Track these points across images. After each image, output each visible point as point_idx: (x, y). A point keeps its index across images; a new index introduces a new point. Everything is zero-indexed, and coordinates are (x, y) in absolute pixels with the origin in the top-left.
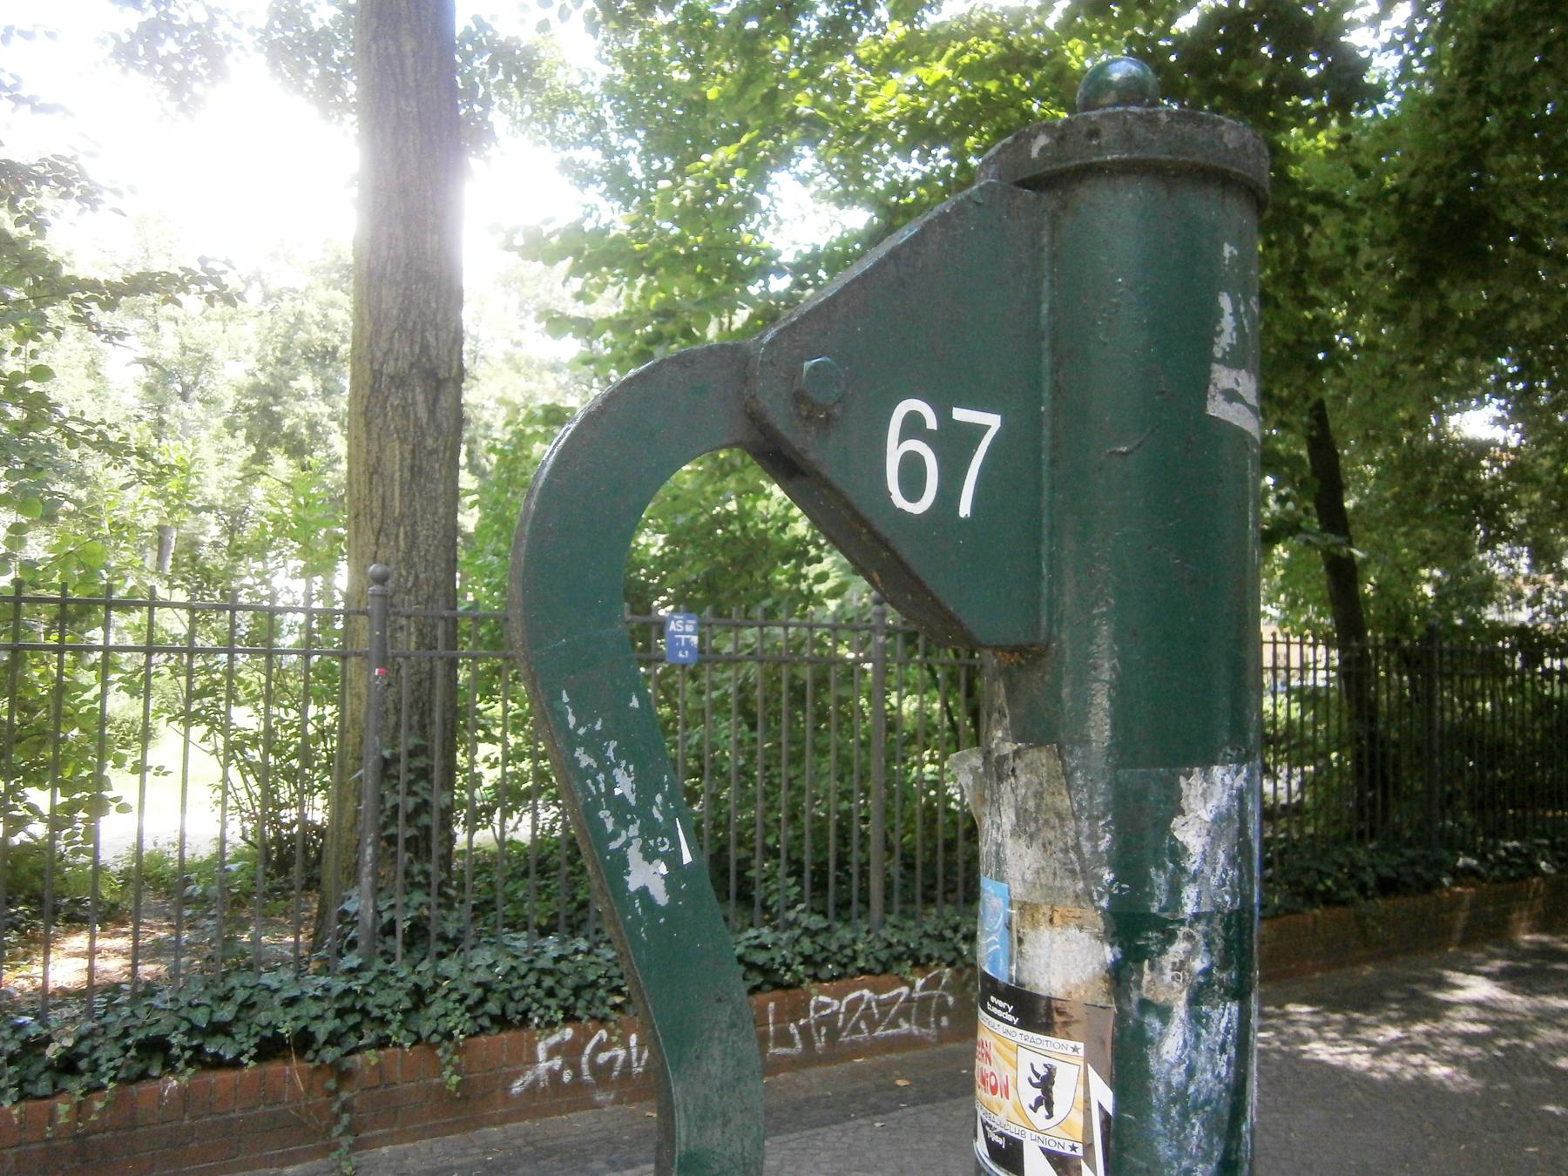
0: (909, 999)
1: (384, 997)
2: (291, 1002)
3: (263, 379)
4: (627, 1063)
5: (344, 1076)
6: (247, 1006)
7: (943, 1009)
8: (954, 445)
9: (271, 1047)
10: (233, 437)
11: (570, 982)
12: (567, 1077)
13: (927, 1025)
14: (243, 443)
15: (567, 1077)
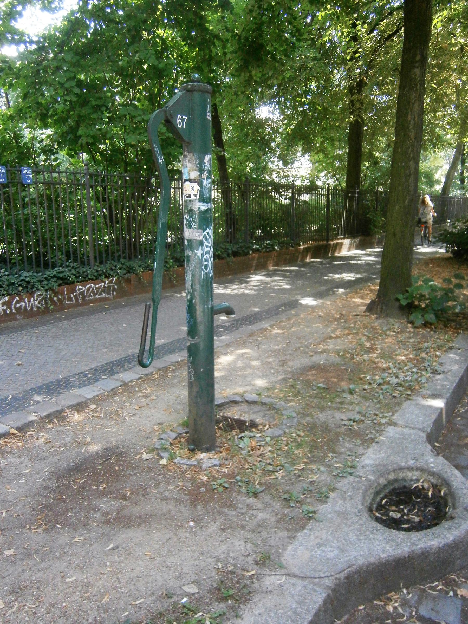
0: (104, 287)
4: (25, 307)
7: (114, 290)
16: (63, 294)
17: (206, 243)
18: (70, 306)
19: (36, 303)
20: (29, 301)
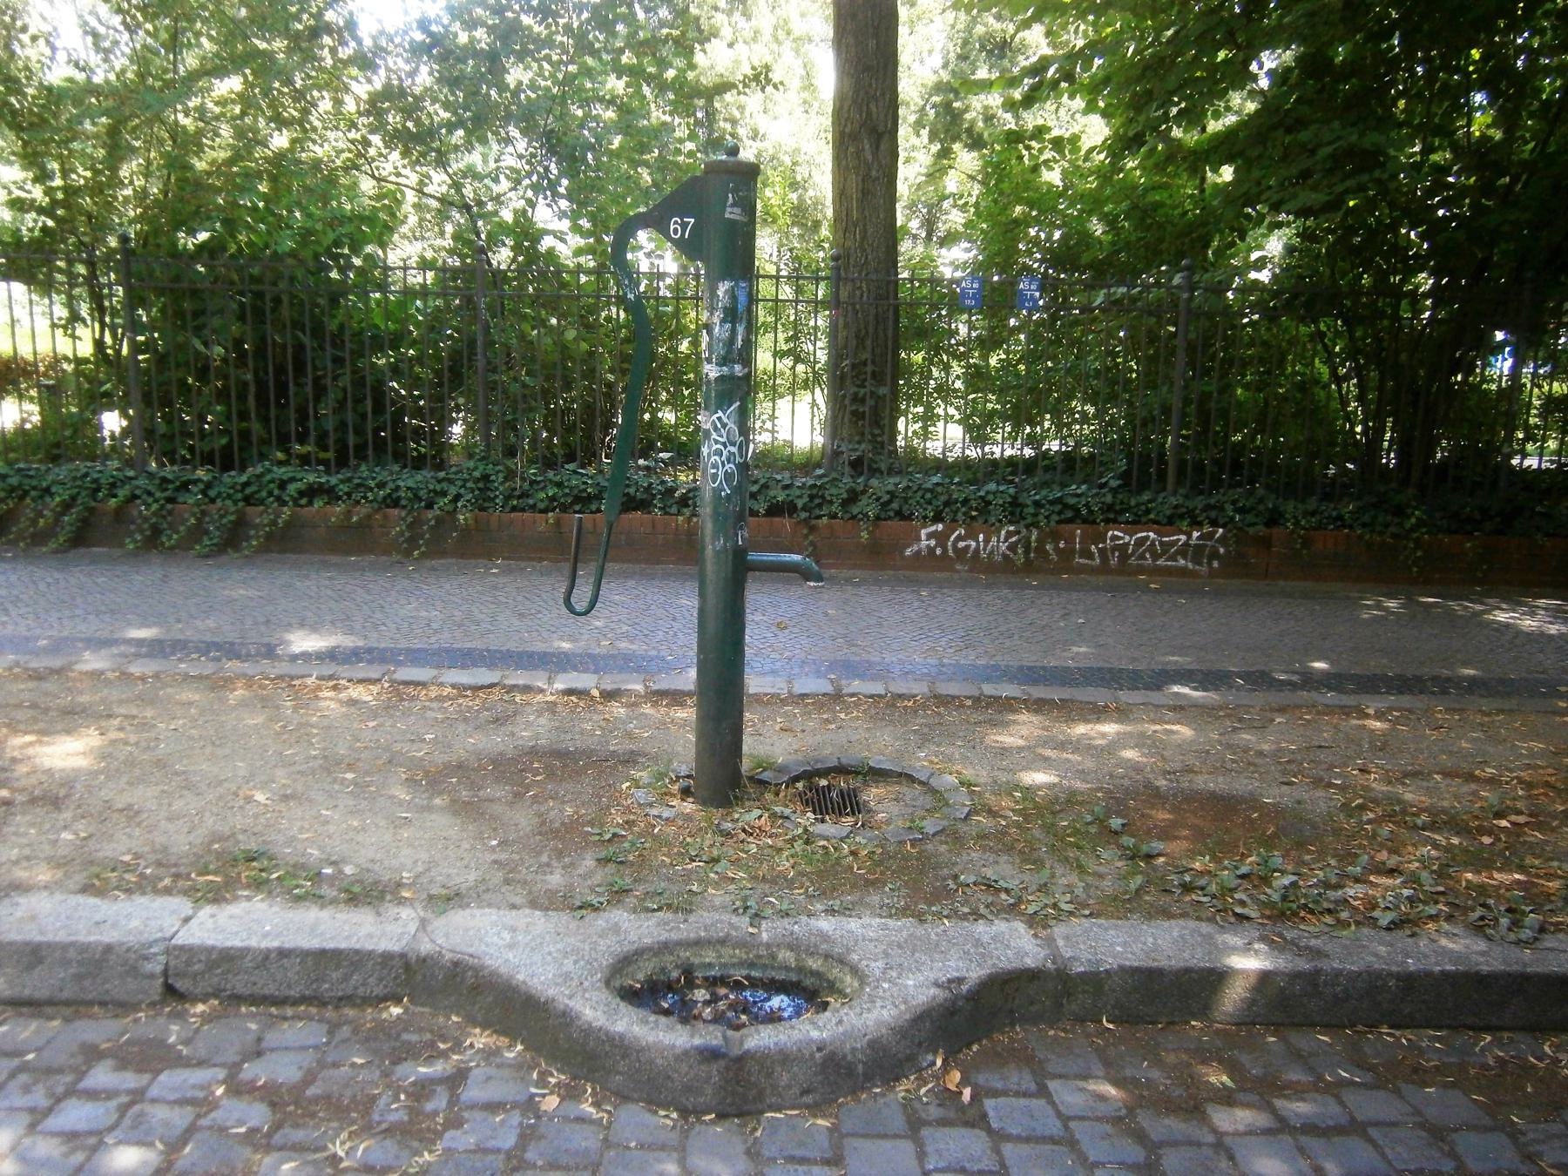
0: (1186, 544)
1: (834, 491)
2: (786, 487)
3: (945, 76)
4: (977, 550)
5: (813, 529)
6: (765, 486)
7: (1214, 555)
8: (684, 225)
9: (775, 510)
10: (918, 135)
11: (943, 498)
12: (938, 551)
13: (1200, 564)
14: (926, 140)
15: (938, 551)
16: (1070, 540)
17: (714, 436)
18: (1082, 569)
19: (1003, 547)
20: (987, 541)
